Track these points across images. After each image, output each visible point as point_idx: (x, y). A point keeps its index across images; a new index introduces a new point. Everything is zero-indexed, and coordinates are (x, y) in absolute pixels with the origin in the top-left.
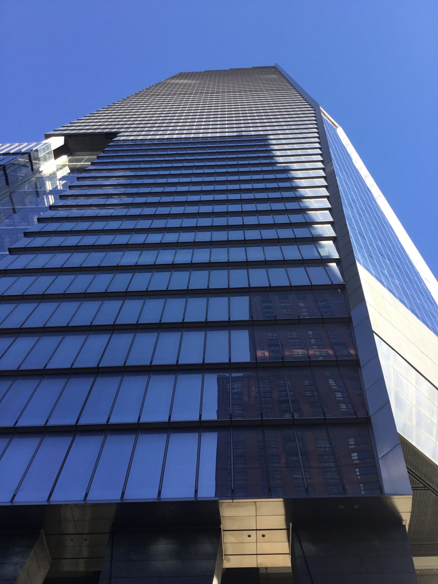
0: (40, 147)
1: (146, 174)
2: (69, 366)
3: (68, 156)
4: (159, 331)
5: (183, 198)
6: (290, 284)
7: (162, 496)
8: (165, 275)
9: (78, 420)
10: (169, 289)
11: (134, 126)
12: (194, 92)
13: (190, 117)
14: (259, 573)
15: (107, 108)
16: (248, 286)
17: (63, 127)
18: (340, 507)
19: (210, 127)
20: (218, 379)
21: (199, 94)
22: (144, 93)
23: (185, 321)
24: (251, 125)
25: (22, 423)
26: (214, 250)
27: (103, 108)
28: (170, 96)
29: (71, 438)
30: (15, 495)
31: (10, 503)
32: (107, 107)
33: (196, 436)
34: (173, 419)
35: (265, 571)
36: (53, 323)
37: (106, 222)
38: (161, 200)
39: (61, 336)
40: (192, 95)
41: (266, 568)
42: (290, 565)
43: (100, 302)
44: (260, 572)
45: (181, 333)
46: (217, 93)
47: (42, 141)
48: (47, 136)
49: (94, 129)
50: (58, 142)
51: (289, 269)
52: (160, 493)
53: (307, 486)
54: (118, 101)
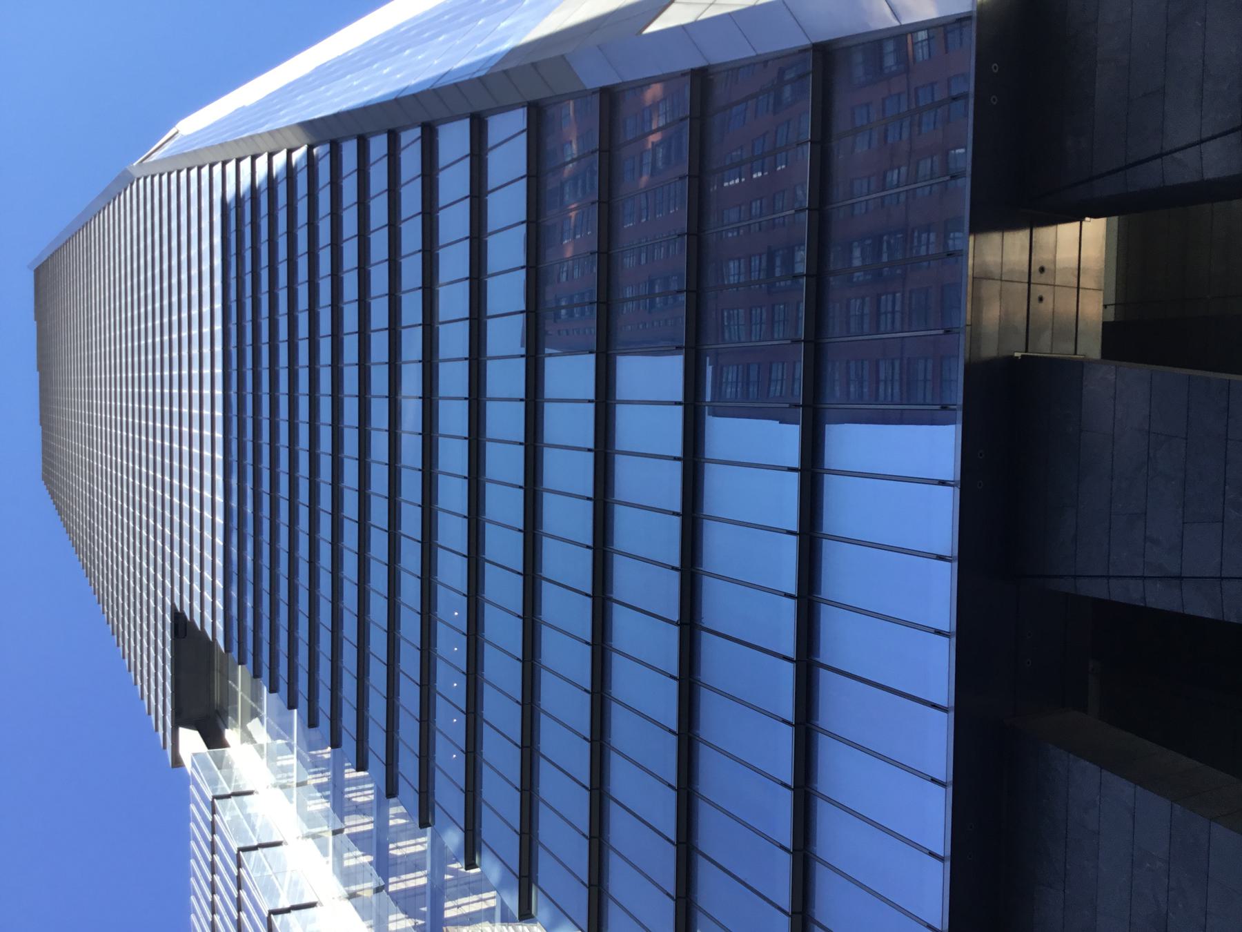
0: (200, 776)
1: (268, 546)
2: (674, 739)
3: (227, 728)
4: (610, 550)
5: (326, 435)
6: (522, 268)
7: (946, 552)
8: (492, 576)
9: (785, 721)
10: (521, 527)
11: (159, 577)
12: (87, 460)
13: (144, 454)
14: (1114, 322)
15: (118, 637)
16: (523, 360)
17: (157, 729)
18: (981, 458)
19: (167, 426)
20: (715, 414)
21: (93, 448)
22: (86, 547)
23: (591, 495)
24: (166, 338)
25: (784, 897)
26: (442, 392)
27: (118, 645)
28: (96, 525)
29: (822, 672)
30: (930, 853)
31: (946, 864)
32: (116, 636)
33: (829, 480)
34: (795, 528)
35: (1111, 310)
36: (583, 771)
37: (372, 657)
38: (327, 510)
39: (607, 902)
40: (93, 464)
41: (1105, 306)
42: (1102, 222)
43: (543, 672)
44: (1112, 319)
45: (616, 505)
46: (90, 407)
47: (187, 772)
48: (177, 762)
49: (164, 661)
50: (190, 741)
51: (490, 270)
52: (941, 558)
53: (947, 175)
54: (103, 613)
